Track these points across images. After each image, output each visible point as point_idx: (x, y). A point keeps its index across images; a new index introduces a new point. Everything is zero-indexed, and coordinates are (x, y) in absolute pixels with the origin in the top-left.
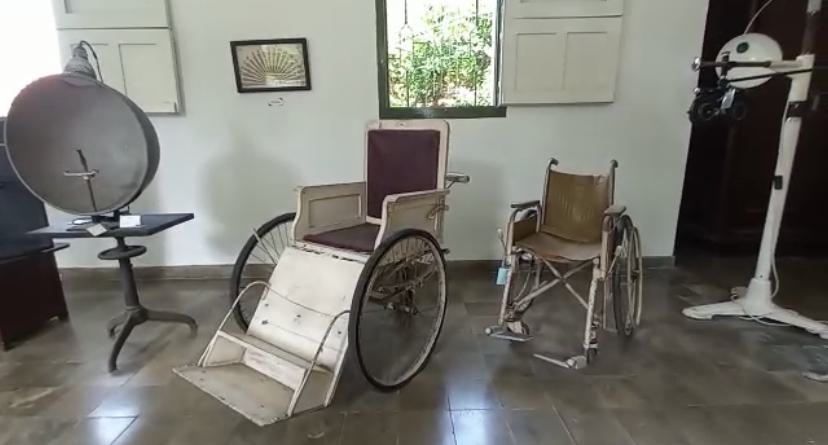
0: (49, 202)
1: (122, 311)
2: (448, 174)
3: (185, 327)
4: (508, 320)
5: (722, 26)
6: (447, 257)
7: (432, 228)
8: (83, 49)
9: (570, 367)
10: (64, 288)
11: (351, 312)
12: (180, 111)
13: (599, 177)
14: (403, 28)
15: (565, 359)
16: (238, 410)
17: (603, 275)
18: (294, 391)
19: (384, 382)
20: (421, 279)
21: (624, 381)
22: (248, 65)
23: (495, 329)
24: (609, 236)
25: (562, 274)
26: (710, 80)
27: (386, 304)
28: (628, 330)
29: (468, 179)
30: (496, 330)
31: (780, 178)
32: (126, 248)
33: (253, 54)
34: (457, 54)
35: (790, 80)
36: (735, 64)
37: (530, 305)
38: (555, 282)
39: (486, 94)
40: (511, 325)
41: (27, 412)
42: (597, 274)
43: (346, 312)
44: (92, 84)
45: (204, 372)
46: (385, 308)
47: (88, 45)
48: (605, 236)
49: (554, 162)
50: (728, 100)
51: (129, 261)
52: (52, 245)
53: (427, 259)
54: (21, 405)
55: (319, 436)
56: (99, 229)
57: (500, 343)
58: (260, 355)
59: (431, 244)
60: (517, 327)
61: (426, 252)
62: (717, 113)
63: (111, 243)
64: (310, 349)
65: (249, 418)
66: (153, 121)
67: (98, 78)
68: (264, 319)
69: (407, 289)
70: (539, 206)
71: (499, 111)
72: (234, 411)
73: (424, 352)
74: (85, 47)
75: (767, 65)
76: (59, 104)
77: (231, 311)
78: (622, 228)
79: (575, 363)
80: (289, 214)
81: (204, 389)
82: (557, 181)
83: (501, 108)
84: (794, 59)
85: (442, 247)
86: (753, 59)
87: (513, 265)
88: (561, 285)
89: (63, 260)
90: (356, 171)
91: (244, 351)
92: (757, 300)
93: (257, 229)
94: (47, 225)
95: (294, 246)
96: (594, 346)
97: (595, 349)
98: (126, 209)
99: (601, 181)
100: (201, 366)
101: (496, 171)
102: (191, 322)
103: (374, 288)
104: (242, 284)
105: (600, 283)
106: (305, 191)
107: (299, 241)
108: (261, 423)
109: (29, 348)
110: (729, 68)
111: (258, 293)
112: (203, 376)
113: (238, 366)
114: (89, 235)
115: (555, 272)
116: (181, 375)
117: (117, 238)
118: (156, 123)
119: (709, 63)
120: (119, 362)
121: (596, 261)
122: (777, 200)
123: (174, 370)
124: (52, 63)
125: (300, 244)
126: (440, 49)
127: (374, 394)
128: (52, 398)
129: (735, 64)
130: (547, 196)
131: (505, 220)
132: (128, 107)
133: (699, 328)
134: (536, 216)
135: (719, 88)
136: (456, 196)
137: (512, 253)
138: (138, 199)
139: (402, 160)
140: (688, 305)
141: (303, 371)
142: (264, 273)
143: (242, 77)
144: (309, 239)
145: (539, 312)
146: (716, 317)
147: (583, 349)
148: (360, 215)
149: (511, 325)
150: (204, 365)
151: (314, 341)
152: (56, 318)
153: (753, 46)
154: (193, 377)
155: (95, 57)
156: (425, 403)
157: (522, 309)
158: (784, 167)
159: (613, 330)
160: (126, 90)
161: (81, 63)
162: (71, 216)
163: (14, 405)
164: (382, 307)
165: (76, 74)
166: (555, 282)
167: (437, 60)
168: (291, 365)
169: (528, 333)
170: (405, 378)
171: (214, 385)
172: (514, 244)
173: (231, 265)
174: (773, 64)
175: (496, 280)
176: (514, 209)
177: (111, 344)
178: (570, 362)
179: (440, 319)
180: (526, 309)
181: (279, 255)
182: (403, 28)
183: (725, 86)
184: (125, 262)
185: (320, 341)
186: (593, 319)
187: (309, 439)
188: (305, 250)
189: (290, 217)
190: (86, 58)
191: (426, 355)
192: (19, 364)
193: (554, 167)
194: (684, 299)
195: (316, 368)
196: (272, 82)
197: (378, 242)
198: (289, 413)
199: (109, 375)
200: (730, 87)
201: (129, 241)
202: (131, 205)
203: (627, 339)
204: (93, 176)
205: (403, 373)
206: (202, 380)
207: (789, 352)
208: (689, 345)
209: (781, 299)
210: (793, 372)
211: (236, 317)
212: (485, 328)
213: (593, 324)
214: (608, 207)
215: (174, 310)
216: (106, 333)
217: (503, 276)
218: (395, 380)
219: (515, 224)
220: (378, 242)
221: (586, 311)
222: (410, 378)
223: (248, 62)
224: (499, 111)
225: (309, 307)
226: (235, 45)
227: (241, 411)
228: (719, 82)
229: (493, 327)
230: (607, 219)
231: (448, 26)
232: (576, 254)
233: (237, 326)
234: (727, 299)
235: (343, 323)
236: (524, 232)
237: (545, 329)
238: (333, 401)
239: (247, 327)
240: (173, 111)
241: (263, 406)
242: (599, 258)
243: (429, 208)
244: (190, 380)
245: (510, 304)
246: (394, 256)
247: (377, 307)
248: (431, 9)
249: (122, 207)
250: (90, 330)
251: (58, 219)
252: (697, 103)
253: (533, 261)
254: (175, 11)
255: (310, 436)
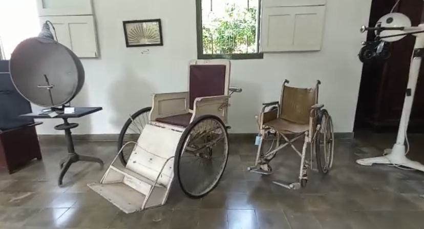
0: (34, 102)
1: (66, 155)
2: (230, 88)
3: (97, 165)
4: (261, 164)
5: (378, 11)
6: (229, 131)
7: (221, 115)
8: (48, 25)
9: (291, 188)
10: (40, 144)
11: (175, 157)
12: (98, 56)
13: (311, 89)
14: (210, 13)
15: (289, 184)
16: (116, 205)
17: (310, 141)
18: (145, 196)
19: (193, 194)
20: (215, 141)
21: (321, 197)
22: (132, 33)
23: (251, 169)
24: (313, 120)
25: (289, 140)
26: (372, 38)
27: (196, 153)
28: (325, 170)
29: (241, 90)
30: (253, 168)
31: (410, 90)
32: (68, 124)
33: (134, 27)
34: (241, 27)
35: (415, 37)
36: (384, 29)
37: (274, 156)
38: (287, 144)
39: (252, 49)
40: (262, 166)
41: (17, 204)
42: (308, 140)
43: (173, 157)
44: (52, 42)
45: (103, 186)
46: (196, 156)
47: (50, 23)
48: (311, 119)
49: (287, 81)
50: (380, 48)
51: (69, 130)
52: (34, 122)
53: (219, 131)
54: (15, 200)
55: (158, 221)
56: (54, 114)
57: (256, 176)
58: (131, 178)
59: (220, 123)
60: (265, 167)
61: (218, 128)
62: (374, 55)
63: (61, 121)
64: (153, 174)
65: (121, 209)
66: (83, 62)
67: (55, 39)
68: (134, 160)
69: (207, 146)
70: (278, 105)
71: (259, 56)
72: (114, 206)
73: (216, 179)
74: (48, 23)
75: (402, 29)
76: (33, 53)
77: (117, 156)
78: (321, 115)
79: (294, 187)
80: (148, 108)
81: (101, 195)
82: (287, 91)
83: (260, 54)
84: (417, 26)
85: (226, 125)
86: (395, 26)
87: (263, 135)
88: (289, 146)
89: (40, 131)
90: (184, 86)
91: (124, 176)
92: (397, 155)
93: (131, 115)
94: (31, 112)
95: (151, 124)
96: (305, 178)
97: (305, 180)
98: (68, 104)
99: (311, 91)
100: (102, 183)
101: (256, 86)
102: (101, 162)
103: (188, 145)
104: (124, 144)
105: (308, 144)
106: (156, 96)
107: (154, 121)
108: (127, 212)
109: (18, 174)
110: (381, 31)
111: (132, 146)
112: (102, 188)
113: (121, 183)
114: (49, 117)
115: (286, 139)
116: (90, 187)
117: (64, 119)
118: (84, 63)
119: (372, 28)
120: (64, 181)
121: (306, 133)
122: (408, 102)
123: (88, 185)
124: (35, 31)
125: (154, 123)
126: (233, 26)
127: (186, 199)
128: (29, 198)
129: (384, 29)
130: (282, 101)
131: (260, 111)
132: (70, 56)
133: (364, 170)
134: (277, 110)
135: (375, 42)
136: (233, 99)
137: (263, 128)
138: (75, 98)
139: (207, 80)
140: (359, 158)
141: (150, 186)
142: (135, 137)
143: (129, 39)
144: (158, 120)
145: (279, 160)
146: (375, 164)
147: (299, 179)
148: (184, 108)
149: (262, 166)
150: (103, 183)
151: (157, 171)
152: (36, 159)
153: (394, 20)
154: (96, 188)
155: (54, 29)
156: (216, 206)
157: (269, 158)
158: (412, 84)
159: (316, 170)
160: (72, 46)
161: (46, 32)
162: (42, 108)
163: (11, 201)
164: (194, 155)
165: (45, 37)
166: (287, 144)
167: (231, 31)
168: (146, 184)
169: (271, 170)
170: (202, 193)
171: (106, 193)
172: (264, 124)
173: (118, 134)
174: (405, 28)
175: (255, 142)
176: (264, 106)
177: (60, 171)
178: (291, 186)
179: (224, 164)
180: (272, 159)
181: (143, 129)
182: (210, 13)
183: (379, 40)
184: (68, 132)
185: (160, 171)
186: (305, 163)
187: (154, 222)
188: (156, 126)
189: (148, 109)
190: (49, 29)
191: (217, 181)
192: (16, 181)
193: (286, 84)
194: (357, 154)
195: (157, 185)
196: (146, 42)
197: (191, 121)
198: (143, 208)
199: (59, 187)
200: (381, 41)
201: (70, 121)
202: (71, 102)
203: (324, 174)
204: (52, 87)
205: (204, 190)
206: (101, 190)
207: (412, 183)
208: (358, 179)
209: (410, 156)
210: (415, 195)
211: (120, 157)
212: (247, 168)
213: (304, 166)
214: (314, 104)
215: (93, 156)
216: (59, 166)
217: (259, 140)
218: (200, 193)
219: (265, 114)
220: (191, 121)
221: (300, 158)
222: (208, 193)
223: (131, 31)
224: (259, 56)
225: (156, 155)
226: (125, 23)
227: (118, 206)
228: (375, 38)
229: (252, 167)
230: (312, 110)
231: (237, 12)
232: (297, 129)
233: (121, 164)
234: (381, 155)
235: (171, 163)
236: (270, 118)
237: (282, 169)
238: (167, 202)
239: (126, 164)
240: (94, 56)
241: (130, 204)
242: (308, 131)
243: (219, 105)
244: (95, 190)
245: (262, 155)
246: (201, 128)
247: (188, 154)
248: (228, 4)
249: (66, 103)
250: (52, 164)
251: (36, 109)
252: (363, 50)
253: (276, 133)
254: (96, 6)
255: (154, 220)
